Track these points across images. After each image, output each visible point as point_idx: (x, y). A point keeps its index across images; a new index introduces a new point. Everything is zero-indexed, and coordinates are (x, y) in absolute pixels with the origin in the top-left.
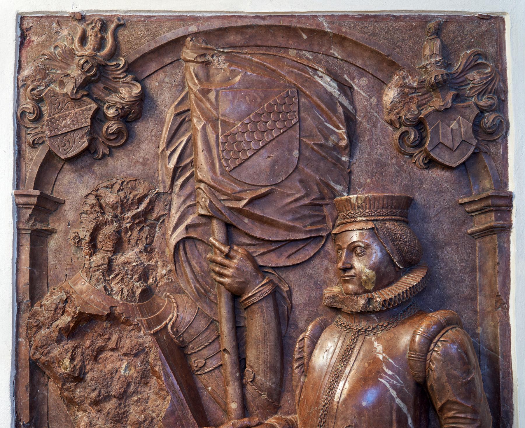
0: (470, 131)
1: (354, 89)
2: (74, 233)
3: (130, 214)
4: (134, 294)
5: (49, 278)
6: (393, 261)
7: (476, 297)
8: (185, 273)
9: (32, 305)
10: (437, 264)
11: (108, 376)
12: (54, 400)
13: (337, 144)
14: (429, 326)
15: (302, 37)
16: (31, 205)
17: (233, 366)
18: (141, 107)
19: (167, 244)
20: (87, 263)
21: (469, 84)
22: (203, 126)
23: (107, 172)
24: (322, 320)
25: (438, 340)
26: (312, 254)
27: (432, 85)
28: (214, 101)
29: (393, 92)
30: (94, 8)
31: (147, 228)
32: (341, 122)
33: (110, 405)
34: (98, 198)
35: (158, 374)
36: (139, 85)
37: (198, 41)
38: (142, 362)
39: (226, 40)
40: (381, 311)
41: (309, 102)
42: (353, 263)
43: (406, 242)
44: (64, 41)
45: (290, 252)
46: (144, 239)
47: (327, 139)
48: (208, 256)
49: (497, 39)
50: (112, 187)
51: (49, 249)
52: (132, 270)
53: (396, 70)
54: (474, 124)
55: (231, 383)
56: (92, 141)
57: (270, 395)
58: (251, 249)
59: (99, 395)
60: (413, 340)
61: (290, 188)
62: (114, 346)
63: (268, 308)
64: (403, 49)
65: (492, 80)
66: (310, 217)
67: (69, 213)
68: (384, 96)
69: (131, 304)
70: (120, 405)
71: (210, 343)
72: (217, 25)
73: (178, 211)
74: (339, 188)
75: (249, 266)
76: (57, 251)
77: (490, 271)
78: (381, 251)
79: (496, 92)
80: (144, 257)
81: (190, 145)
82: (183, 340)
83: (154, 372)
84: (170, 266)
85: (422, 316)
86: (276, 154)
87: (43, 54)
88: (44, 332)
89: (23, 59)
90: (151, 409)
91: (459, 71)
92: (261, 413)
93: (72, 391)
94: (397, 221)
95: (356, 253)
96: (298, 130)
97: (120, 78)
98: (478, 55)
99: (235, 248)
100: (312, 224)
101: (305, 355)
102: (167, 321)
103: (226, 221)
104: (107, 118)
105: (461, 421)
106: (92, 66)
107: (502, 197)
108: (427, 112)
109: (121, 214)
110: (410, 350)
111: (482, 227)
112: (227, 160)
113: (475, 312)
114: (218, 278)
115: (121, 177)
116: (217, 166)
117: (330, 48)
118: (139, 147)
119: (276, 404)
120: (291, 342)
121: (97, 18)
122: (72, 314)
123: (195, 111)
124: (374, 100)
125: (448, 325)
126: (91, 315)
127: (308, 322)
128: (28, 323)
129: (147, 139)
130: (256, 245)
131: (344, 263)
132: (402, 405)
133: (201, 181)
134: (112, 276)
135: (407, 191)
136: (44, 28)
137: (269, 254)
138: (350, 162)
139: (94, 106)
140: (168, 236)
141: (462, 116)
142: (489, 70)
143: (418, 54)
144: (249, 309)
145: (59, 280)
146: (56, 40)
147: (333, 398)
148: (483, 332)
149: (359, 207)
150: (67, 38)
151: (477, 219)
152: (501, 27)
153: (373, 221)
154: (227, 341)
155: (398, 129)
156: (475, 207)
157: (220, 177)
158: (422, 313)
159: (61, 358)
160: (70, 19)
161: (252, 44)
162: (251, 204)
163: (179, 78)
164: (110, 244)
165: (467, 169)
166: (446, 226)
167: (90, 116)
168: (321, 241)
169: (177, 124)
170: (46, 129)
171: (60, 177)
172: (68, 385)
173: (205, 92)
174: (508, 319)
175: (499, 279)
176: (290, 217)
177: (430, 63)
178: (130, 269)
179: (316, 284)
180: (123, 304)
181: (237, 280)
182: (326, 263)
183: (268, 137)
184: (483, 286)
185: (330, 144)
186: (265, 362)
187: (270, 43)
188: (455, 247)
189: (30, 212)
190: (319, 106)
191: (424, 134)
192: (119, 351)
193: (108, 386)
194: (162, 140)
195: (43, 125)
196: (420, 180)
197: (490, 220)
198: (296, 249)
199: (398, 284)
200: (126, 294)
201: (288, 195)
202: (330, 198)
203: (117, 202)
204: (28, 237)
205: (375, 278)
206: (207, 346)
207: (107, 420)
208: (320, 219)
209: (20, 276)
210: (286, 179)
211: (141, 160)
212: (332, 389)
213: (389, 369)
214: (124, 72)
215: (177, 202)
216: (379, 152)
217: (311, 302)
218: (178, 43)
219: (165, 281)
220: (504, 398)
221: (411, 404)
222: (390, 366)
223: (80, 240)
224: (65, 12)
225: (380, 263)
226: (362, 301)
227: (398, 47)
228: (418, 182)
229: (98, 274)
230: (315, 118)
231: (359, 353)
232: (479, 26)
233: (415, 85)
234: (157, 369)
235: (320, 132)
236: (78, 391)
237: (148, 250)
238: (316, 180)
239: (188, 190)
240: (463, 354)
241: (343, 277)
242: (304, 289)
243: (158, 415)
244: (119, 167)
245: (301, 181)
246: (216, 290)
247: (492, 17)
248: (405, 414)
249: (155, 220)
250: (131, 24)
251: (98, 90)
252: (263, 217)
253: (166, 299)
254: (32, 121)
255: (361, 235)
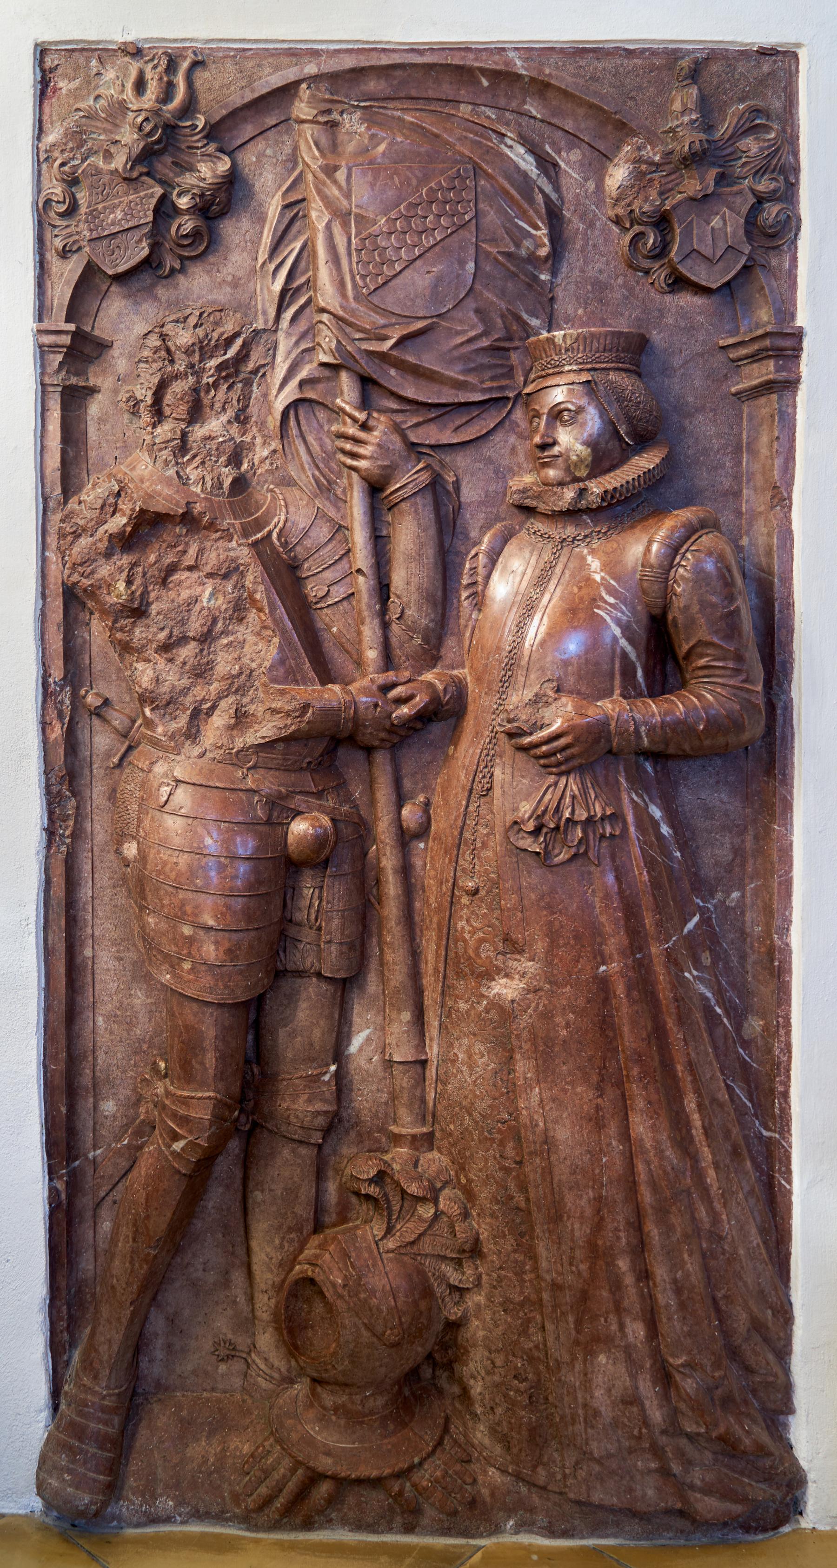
0: (741, 232)
1: (560, 167)
2: (128, 392)
3: (213, 363)
4: (221, 485)
5: (90, 462)
6: (618, 432)
7: (741, 491)
8: (298, 454)
9: (66, 502)
10: (682, 440)
11: (183, 608)
12: (99, 646)
13: (533, 253)
14: (673, 530)
15: (480, 83)
16: (62, 347)
17: (370, 595)
18: (230, 194)
19: (269, 410)
20: (148, 438)
21: (741, 158)
22: (327, 224)
23: (177, 298)
24: (505, 526)
25: (687, 550)
26: (492, 426)
27: (685, 159)
28: (343, 184)
29: (621, 171)
30: (156, 35)
31: (240, 385)
32: (540, 218)
33: (187, 652)
34: (163, 337)
35: (259, 604)
36: (227, 159)
37: (318, 89)
38: (235, 587)
39: (363, 87)
40: (600, 509)
41: (492, 186)
42: (556, 436)
43: (639, 403)
44: (109, 88)
45: (458, 422)
46: (235, 402)
47: (518, 245)
48: (333, 429)
49: (785, 87)
50: (185, 322)
51: (89, 418)
52: (217, 449)
53: (627, 135)
54: (747, 222)
55: (368, 620)
56: (155, 246)
57: (426, 639)
58: (399, 418)
59: (170, 637)
60: (648, 550)
61: (461, 322)
62: (192, 563)
63: (425, 505)
64: (639, 102)
65: (777, 151)
66: (490, 367)
67: (119, 360)
68: (607, 177)
69: (217, 499)
70: (202, 650)
71: (336, 561)
72: (349, 62)
73: (287, 358)
74: (535, 322)
75: (396, 443)
76: (101, 420)
77: (764, 451)
78: (601, 417)
79: (783, 170)
80: (234, 430)
81: (305, 254)
82: (295, 556)
83: (254, 602)
84: (275, 444)
85: (661, 517)
86: (440, 267)
87: (78, 110)
88: (85, 541)
89: (45, 118)
90: (248, 657)
91: (726, 137)
92: (413, 667)
93: (129, 631)
94: (625, 370)
95: (561, 421)
96: (474, 229)
97: (197, 148)
98: (757, 111)
99: (375, 415)
100: (493, 379)
101: (480, 579)
102: (271, 526)
103: (362, 372)
104: (177, 211)
105: (717, 672)
106: (155, 128)
107: (787, 334)
108: (675, 202)
109: (200, 362)
110: (643, 566)
111: (755, 382)
112: (364, 277)
113: (739, 513)
114: (349, 462)
115: (198, 305)
116: (349, 286)
117: (524, 102)
118: (226, 259)
119: (434, 652)
120: (458, 560)
121: (161, 51)
122: (128, 512)
123: (315, 201)
124: (591, 185)
125: (702, 527)
126: (158, 514)
127: (484, 529)
128: (60, 528)
129: (238, 246)
130: (406, 411)
131: (542, 437)
132: (629, 649)
133: (323, 310)
134: (187, 457)
135: (639, 327)
136: (77, 68)
137: (425, 426)
138: (552, 283)
139: (158, 191)
140: (272, 397)
141: (731, 209)
142: (772, 135)
143: (662, 110)
144: (396, 509)
145: (106, 465)
146: (97, 87)
147: (523, 639)
148: (751, 544)
149: (567, 350)
150: (114, 82)
151: (746, 370)
152: (793, 68)
153: (589, 370)
154: (362, 557)
155: (628, 230)
156: (743, 351)
157: (354, 305)
158: (659, 512)
159: (112, 579)
160: (119, 53)
161: (402, 95)
162: (401, 346)
163: (288, 150)
164: (182, 410)
165: (730, 293)
166: (697, 383)
167: (152, 207)
168: (505, 406)
169: (286, 221)
170: (83, 226)
171: (104, 305)
172: (123, 622)
173: (330, 170)
174: (790, 524)
175: (778, 462)
176: (459, 367)
177: (682, 124)
178: (214, 447)
179: (496, 472)
180: (206, 498)
181: (380, 463)
182: (512, 439)
183: (427, 241)
184: (753, 474)
185: (523, 252)
186: (419, 588)
187: (431, 94)
188: (711, 414)
189: (60, 358)
190: (506, 193)
191: (668, 238)
192: (200, 570)
193: (183, 623)
194: (262, 247)
195: (80, 220)
196: (660, 310)
197: (767, 370)
198: (468, 418)
199: (625, 468)
200: (209, 484)
201: (458, 333)
202: (521, 339)
203: (193, 344)
204: (58, 397)
205: (590, 459)
206: (331, 565)
207: (182, 674)
208: (505, 370)
209: (47, 457)
210: (454, 307)
211: (229, 278)
212: (521, 627)
213: (611, 595)
214: (205, 137)
215: (285, 345)
216: (598, 266)
217: (488, 500)
218: (288, 91)
219: (267, 466)
220: (780, 642)
221: (642, 648)
222: (612, 591)
223: (137, 403)
224: (110, 42)
225: (599, 435)
226: (569, 494)
227: (631, 98)
228: (656, 314)
229: (165, 454)
230: (501, 211)
231: (563, 572)
232: (758, 66)
233: (657, 158)
234: (258, 596)
235: (507, 233)
236: (137, 631)
237: (241, 419)
238: (501, 309)
239: (302, 325)
240: (725, 571)
241: (539, 458)
242: (479, 480)
243: (260, 666)
244: (196, 289)
245: (477, 311)
246: (345, 481)
247: (778, 52)
248: (633, 663)
249: (251, 372)
250: (214, 62)
251: (164, 165)
252: (419, 366)
253: (269, 495)
254: (62, 215)
255: (570, 391)
